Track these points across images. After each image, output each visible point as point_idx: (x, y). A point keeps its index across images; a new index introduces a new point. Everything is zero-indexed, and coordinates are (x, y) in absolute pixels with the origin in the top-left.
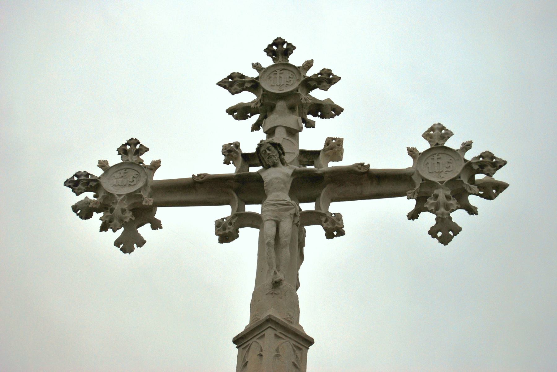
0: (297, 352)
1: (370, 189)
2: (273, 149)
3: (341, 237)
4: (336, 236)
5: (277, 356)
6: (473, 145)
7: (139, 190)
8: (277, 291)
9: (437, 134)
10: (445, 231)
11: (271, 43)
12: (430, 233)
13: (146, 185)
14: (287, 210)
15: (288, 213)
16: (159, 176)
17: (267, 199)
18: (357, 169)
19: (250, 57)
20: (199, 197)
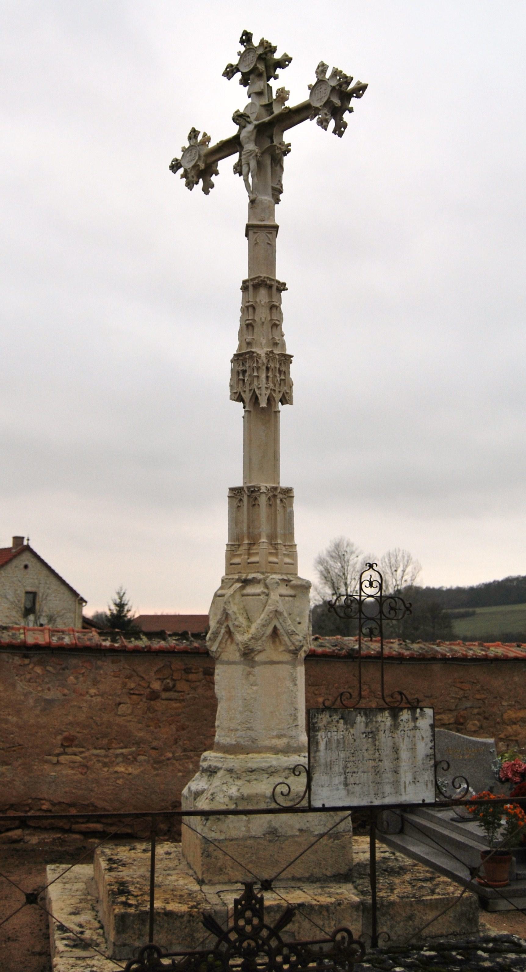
0: (269, 235)
1: (297, 119)
2: (239, 119)
3: (366, 90)
4: (363, 93)
5: (256, 244)
6: (180, 177)
7: (197, 162)
8: (255, 205)
9: (322, 68)
10: (339, 130)
11: (241, 36)
12: (333, 132)
13: (200, 156)
14: (251, 155)
15: (251, 157)
16: (212, 144)
17: (244, 150)
18: (284, 112)
19: (232, 53)
20: (226, 153)
